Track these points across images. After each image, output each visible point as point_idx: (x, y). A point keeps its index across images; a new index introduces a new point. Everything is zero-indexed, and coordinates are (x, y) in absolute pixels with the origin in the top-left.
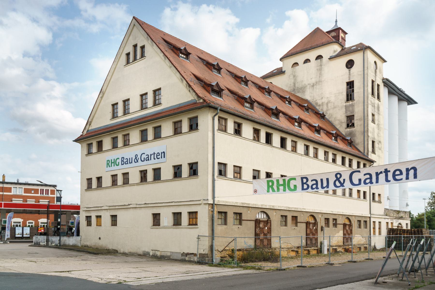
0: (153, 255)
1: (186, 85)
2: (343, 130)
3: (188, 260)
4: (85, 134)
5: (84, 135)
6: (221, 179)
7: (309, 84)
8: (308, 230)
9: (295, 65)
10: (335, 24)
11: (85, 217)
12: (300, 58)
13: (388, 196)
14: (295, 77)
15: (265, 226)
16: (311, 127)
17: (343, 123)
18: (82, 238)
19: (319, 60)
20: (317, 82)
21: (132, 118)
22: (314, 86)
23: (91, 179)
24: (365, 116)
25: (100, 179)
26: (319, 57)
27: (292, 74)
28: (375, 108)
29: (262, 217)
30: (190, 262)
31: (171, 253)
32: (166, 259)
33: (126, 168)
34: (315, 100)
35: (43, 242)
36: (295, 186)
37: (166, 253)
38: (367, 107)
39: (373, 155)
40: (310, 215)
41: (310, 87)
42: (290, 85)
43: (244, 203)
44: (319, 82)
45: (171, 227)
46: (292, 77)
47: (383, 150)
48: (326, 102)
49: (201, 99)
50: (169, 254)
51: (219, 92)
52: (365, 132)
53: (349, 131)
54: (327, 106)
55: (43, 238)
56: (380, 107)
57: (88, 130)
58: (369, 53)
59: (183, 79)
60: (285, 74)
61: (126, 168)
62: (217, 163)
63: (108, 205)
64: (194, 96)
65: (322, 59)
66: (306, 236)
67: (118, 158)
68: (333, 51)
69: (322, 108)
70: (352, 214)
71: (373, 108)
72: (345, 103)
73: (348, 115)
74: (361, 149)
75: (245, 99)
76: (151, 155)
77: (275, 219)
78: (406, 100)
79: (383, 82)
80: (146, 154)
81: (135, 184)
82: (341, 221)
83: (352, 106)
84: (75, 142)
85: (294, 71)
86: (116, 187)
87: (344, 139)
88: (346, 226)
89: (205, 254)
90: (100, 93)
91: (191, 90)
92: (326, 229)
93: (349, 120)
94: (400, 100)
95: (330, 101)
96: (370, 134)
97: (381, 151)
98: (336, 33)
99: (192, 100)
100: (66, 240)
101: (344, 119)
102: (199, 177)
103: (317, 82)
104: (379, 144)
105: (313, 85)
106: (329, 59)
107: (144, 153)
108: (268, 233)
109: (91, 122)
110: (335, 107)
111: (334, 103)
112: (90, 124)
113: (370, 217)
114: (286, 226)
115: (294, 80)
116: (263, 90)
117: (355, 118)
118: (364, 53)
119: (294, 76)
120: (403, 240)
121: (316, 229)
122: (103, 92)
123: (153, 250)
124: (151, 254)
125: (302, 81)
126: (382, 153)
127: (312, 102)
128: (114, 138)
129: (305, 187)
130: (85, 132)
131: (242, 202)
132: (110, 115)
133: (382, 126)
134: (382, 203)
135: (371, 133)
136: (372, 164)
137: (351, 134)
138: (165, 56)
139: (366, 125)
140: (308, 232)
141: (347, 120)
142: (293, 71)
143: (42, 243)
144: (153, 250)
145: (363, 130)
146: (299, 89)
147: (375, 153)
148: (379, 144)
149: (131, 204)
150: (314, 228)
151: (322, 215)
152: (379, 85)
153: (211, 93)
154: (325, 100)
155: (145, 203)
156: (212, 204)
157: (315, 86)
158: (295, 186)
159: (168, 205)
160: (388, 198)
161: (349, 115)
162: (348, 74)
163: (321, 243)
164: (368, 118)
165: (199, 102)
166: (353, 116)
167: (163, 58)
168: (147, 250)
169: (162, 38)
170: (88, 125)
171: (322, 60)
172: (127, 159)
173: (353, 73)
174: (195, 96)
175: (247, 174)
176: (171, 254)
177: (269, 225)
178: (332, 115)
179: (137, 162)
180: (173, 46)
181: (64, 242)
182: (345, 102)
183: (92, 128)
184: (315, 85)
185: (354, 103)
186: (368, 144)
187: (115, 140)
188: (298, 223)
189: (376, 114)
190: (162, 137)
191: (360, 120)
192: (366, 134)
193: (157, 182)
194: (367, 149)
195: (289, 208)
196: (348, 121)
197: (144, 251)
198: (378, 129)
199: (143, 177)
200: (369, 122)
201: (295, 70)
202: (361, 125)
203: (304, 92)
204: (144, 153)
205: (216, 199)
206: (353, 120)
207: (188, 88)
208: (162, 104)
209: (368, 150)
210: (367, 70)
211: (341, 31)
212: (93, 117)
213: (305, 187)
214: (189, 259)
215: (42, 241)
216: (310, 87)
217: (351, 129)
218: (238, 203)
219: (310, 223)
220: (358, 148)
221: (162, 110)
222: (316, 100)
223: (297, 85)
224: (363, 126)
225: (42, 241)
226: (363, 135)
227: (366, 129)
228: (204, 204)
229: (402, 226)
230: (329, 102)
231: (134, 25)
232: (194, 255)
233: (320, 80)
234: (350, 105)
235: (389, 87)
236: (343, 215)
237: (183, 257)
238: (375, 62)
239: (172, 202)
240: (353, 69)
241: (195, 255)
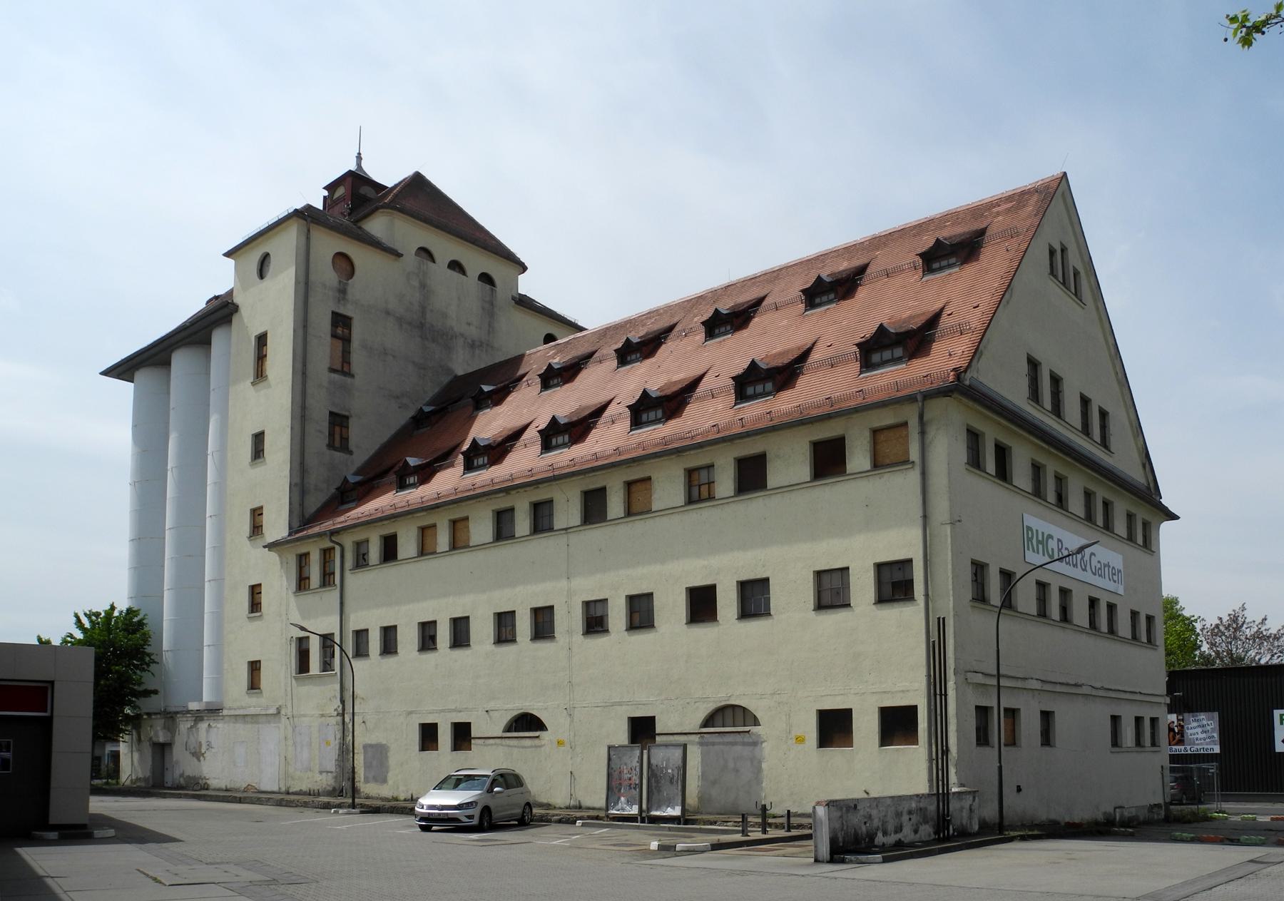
23: (881, 599)
25: (304, 641)
35: (890, 827)
55: (893, 808)
62: (998, 573)
128: (501, 512)
143: (885, 833)
187: (426, 532)
201: (425, 267)
215: (884, 823)
225: (884, 823)
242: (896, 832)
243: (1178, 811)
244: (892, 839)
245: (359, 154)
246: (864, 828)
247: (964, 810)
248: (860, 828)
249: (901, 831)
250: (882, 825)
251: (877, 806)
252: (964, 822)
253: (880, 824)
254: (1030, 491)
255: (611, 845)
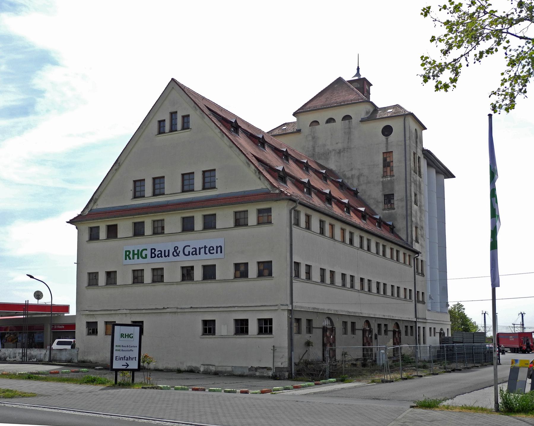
0: (205, 370)
1: (255, 170)
2: (380, 213)
3: (258, 376)
4: (86, 214)
5: (84, 215)
6: (299, 282)
7: (334, 150)
8: (365, 338)
9: (314, 124)
10: (356, 72)
11: (85, 324)
12: (322, 116)
13: (430, 295)
14: (315, 139)
15: (331, 335)
16: (357, 211)
17: (379, 202)
18: (79, 351)
19: (347, 121)
20: (344, 149)
21: (168, 201)
22: (341, 153)
24: (408, 196)
25: (112, 275)
26: (347, 118)
27: (311, 135)
28: (417, 187)
29: (326, 323)
30: (262, 377)
31: (233, 368)
32: (226, 376)
33: (158, 263)
34: (342, 171)
35: (12, 356)
36: (146, 255)
37: (225, 368)
38: (409, 186)
39: (416, 244)
40: (327, 317)
41: (336, 153)
42: (308, 148)
43: (314, 308)
44: (347, 148)
45: (232, 336)
46: (310, 138)
47: (425, 237)
48: (357, 174)
49: (276, 189)
50: (229, 369)
51: (282, 177)
52: (408, 215)
53: (388, 213)
54: (358, 180)
56: (421, 185)
57: (91, 209)
58: (410, 120)
59: (250, 163)
60: (300, 133)
61: (158, 263)
63: (127, 308)
64: (266, 185)
65: (350, 120)
66: (440, 344)
67: (146, 250)
68: (365, 112)
69: (352, 181)
70: (401, 318)
71: (415, 186)
72: (382, 178)
73: (385, 194)
74: (404, 237)
75: (305, 184)
76: (200, 249)
77: (338, 326)
78: (443, 173)
79: (423, 154)
80: (192, 247)
81: (175, 283)
82: (360, 325)
83: (392, 182)
84: (70, 224)
85: (314, 131)
86: (142, 285)
87: (380, 223)
88: (366, 332)
89: (283, 368)
90: (115, 165)
91: (262, 177)
92: (379, 337)
93: (387, 200)
94: (437, 172)
95: (362, 173)
96: (413, 219)
97: (423, 238)
98: (359, 84)
99: (262, 188)
100: (56, 354)
101: (381, 198)
102: (273, 278)
103: (345, 149)
104: (421, 230)
105: (340, 151)
106: (360, 121)
107: (189, 246)
108: (333, 342)
109: (97, 200)
110: (369, 182)
111: (367, 177)
112: (95, 202)
113: (416, 322)
114: (345, 334)
115: (313, 143)
116: (302, 165)
117: (395, 198)
118: (404, 119)
119: (314, 138)
120: (446, 350)
121: (371, 337)
122: (119, 163)
123: (204, 365)
124: (202, 369)
125: (324, 145)
126: (424, 241)
127: (339, 173)
129: (153, 255)
130: (87, 212)
131: (312, 307)
132: (131, 194)
133: (423, 208)
134: (425, 304)
135: (414, 217)
136: (417, 255)
137: (392, 217)
138: (222, 133)
139: (409, 207)
140: (365, 341)
141: (384, 200)
142: (312, 130)
143: (10, 358)
144: (204, 365)
145: (405, 213)
146: (320, 155)
147: (418, 241)
148: (421, 230)
149: (168, 308)
150: (370, 336)
151: (375, 320)
152: (419, 157)
153: (278, 180)
154: (355, 172)
155: (191, 307)
156: (290, 310)
157: (342, 154)
158: (146, 255)
159: (228, 309)
160: (430, 297)
161: (387, 193)
162: (385, 142)
163: (376, 354)
164: (411, 199)
165: (273, 192)
166: (392, 195)
167: (220, 135)
168: (198, 365)
169: (205, 106)
170: (92, 204)
171: (351, 121)
172: (161, 251)
173: (392, 142)
174: (268, 185)
175: (316, 276)
176: (233, 369)
177: (334, 333)
178: (365, 192)
179: (178, 255)
180: (222, 117)
181: (53, 356)
182: (381, 177)
183: (98, 207)
184: (342, 152)
185: (394, 179)
186: (412, 231)
188: (313, 329)
189: (418, 193)
190: (217, 228)
191: (401, 200)
192: (409, 218)
193: (209, 281)
194: (411, 237)
195: (349, 312)
196: (386, 200)
197: (189, 366)
198: (420, 212)
199: (186, 275)
200: (412, 204)
201: (314, 129)
202: (402, 207)
203: (327, 159)
204: (189, 246)
205: (294, 304)
206: (392, 200)
207: (258, 174)
208: (217, 188)
209: (412, 239)
210: (409, 141)
211: (365, 82)
212: (101, 193)
213: (153, 255)
214: (261, 374)
216: (336, 153)
217: (390, 211)
218: (310, 307)
219: (366, 330)
220: (400, 235)
221: (218, 195)
222: (344, 171)
223: (317, 150)
224: (405, 208)
226: (406, 220)
227: (409, 212)
228: (282, 310)
229: (444, 332)
230: (361, 175)
231: (173, 88)
232: (268, 369)
233: (348, 146)
234: (388, 181)
235: (427, 159)
236: (404, 321)
237: (251, 373)
238: (416, 129)
239: (234, 307)
240: (392, 137)
241: (269, 369)
242: (14, 358)
243: (304, 385)
244: (13, 359)
245: (358, 67)
246: (3, 356)
247: (42, 355)
248: (2, 356)
249: (16, 358)
250: (9, 356)
251: (7, 351)
252: (42, 358)
253: (8, 355)
254: (403, 263)
255: (23, 395)
